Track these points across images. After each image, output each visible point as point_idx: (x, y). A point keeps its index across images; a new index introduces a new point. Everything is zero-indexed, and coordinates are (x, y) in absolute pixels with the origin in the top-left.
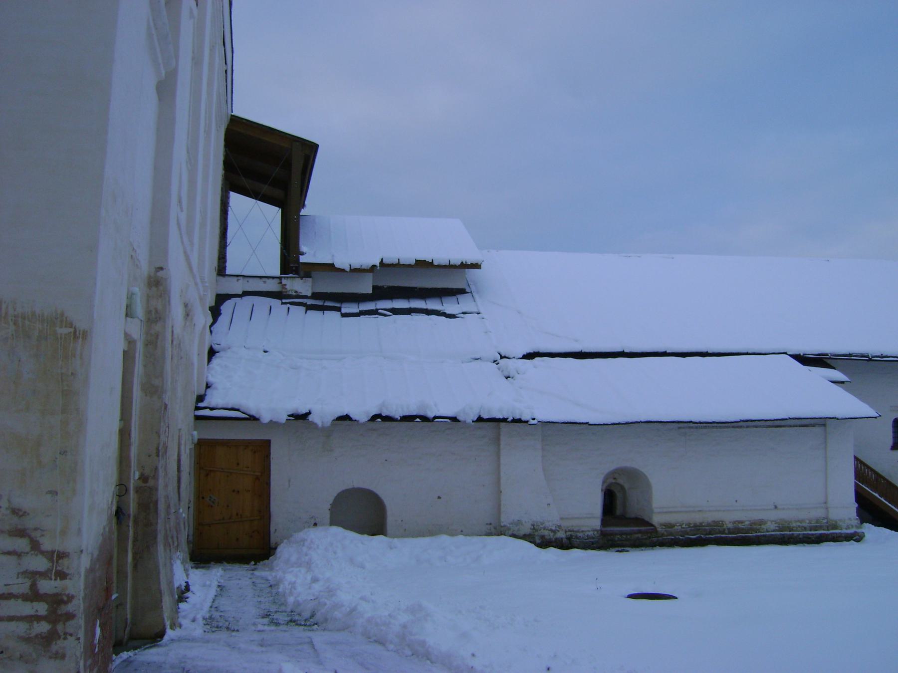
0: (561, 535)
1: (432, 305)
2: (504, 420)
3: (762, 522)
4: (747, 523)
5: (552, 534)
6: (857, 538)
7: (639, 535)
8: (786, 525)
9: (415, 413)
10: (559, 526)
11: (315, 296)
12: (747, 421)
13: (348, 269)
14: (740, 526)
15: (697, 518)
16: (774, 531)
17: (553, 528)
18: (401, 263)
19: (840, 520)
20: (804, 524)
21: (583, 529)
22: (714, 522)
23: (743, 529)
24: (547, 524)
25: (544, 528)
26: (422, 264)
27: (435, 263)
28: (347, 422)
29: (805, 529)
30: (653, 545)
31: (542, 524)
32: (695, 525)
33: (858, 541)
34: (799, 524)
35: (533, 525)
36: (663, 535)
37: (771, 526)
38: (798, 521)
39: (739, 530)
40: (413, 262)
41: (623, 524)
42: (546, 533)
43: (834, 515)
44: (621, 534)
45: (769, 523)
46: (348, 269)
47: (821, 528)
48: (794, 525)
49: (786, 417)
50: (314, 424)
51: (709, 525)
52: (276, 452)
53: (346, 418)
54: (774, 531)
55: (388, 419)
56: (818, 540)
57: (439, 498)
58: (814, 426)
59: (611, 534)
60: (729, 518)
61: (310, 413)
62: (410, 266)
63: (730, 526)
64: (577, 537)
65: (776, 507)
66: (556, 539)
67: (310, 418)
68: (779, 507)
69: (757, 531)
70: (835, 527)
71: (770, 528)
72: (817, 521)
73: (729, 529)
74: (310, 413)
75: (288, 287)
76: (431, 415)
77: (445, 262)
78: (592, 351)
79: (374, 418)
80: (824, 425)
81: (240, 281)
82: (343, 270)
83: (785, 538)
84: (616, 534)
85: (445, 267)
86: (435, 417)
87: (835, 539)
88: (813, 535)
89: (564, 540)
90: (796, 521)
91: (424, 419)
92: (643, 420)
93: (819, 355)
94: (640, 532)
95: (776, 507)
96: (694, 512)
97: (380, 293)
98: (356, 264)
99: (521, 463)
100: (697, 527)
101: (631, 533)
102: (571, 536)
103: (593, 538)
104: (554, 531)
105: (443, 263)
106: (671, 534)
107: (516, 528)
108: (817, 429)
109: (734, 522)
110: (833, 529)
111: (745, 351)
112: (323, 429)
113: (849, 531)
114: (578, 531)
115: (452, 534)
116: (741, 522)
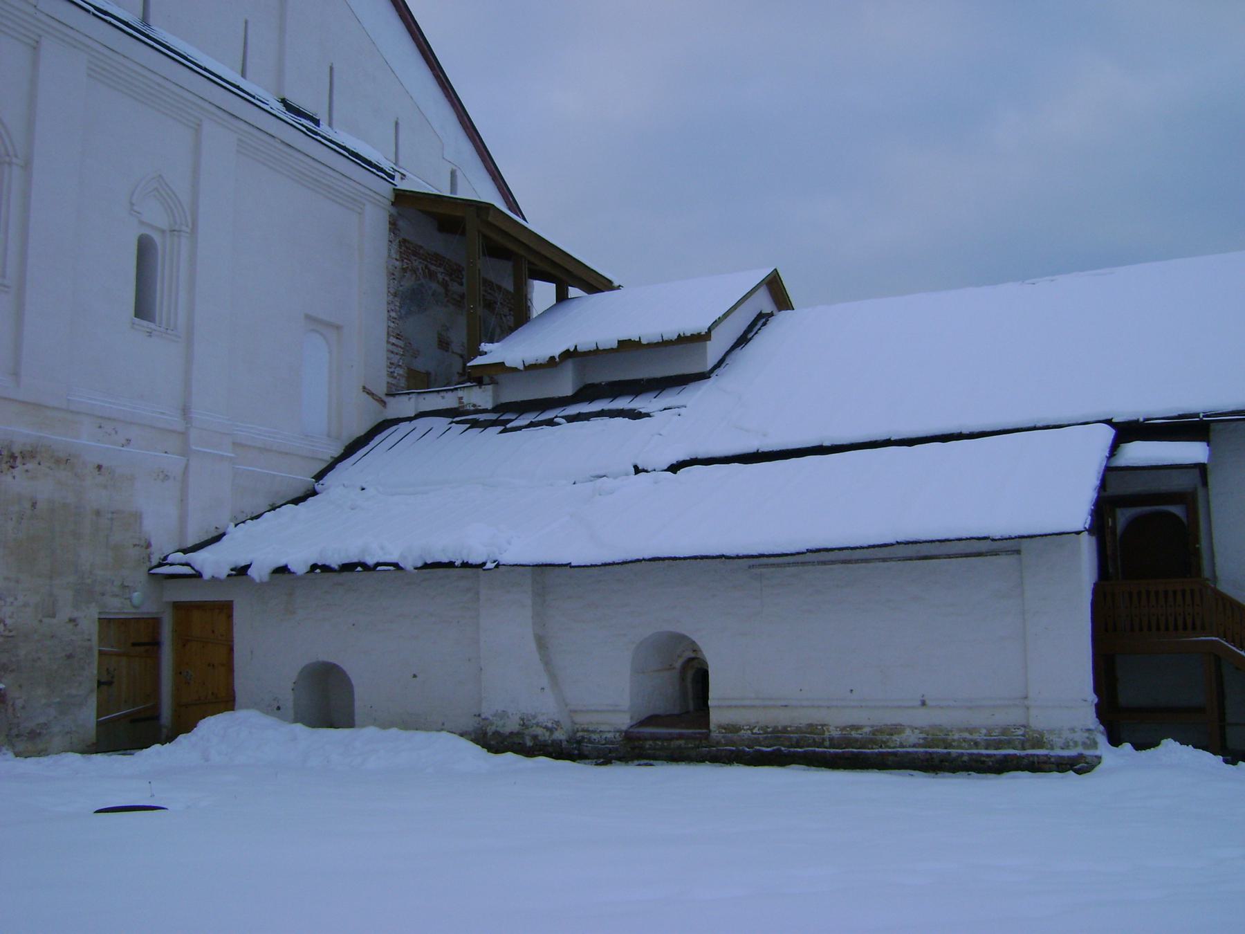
0: (560, 735)
1: (623, 403)
2: (451, 565)
3: (896, 729)
4: (867, 730)
5: (547, 734)
6: (1079, 765)
7: (682, 742)
8: (942, 736)
9: (355, 560)
10: (557, 723)
11: (500, 408)
12: (818, 550)
13: (521, 368)
14: (854, 734)
15: (782, 718)
16: (914, 746)
17: (550, 725)
18: (601, 348)
19: (1051, 731)
20: (976, 736)
21: (603, 728)
22: (810, 725)
23: (856, 740)
24: (541, 718)
25: (537, 725)
26: (626, 346)
27: (644, 341)
28: (285, 576)
29: (976, 744)
30: (700, 759)
31: (534, 717)
32: (775, 730)
33: (1079, 772)
34: (966, 735)
35: (523, 719)
36: (718, 743)
37: (910, 737)
38: (967, 730)
39: (849, 742)
40: (615, 345)
41: (681, 725)
42: (539, 731)
43: (1039, 721)
44: (655, 738)
45: (908, 732)
46: (521, 368)
47: (1009, 744)
48: (956, 736)
49: (892, 541)
50: (253, 580)
51: (798, 730)
52: (237, 614)
53: (283, 570)
54: (914, 746)
55: (326, 568)
56: (1001, 766)
57: (415, 676)
58: (995, 553)
59: (639, 739)
60: (836, 720)
61: (248, 566)
62: (612, 350)
63: (836, 734)
64: (590, 741)
65: (923, 703)
66: (553, 741)
67: (250, 572)
68: (928, 702)
69: (883, 744)
70: (1039, 743)
71: (909, 740)
72: (1005, 731)
73: (831, 739)
74: (248, 566)
75: (465, 401)
76: (371, 561)
77: (657, 339)
78: (845, 443)
79: (314, 567)
80: (1018, 552)
81: (413, 400)
82: (515, 370)
83: (937, 759)
84: (646, 739)
85: (657, 345)
86: (378, 564)
87: (1036, 766)
88: (988, 756)
89: (564, 744)
90: (960, 730)
91: (365, 567)
92: (646, 557)
93: (1180, 417)
94: (680, 736)
95: (923, 703)
96: (774, 707)
97: (587, 393)
98: (530, 360)
99: (508, 626)
100: (778, 734)
101: (671, 738)
102: (583, 737)
103: (612, 743)
104: (551, 730)
105: (608, 347)
106: (732, 743)
107: (501, 723)
108: (1003, 560)
109: (844, 728)
110: (1033, 747)
111: (1031, 425)
112: (262, 584)
113: (1066, 753)
114: (594, 732)
115: (385, 725)
116: (856, 728)
